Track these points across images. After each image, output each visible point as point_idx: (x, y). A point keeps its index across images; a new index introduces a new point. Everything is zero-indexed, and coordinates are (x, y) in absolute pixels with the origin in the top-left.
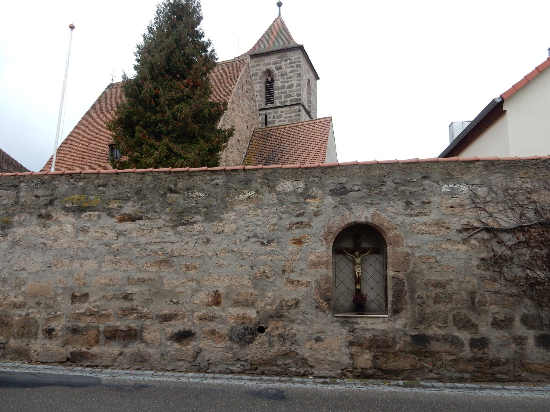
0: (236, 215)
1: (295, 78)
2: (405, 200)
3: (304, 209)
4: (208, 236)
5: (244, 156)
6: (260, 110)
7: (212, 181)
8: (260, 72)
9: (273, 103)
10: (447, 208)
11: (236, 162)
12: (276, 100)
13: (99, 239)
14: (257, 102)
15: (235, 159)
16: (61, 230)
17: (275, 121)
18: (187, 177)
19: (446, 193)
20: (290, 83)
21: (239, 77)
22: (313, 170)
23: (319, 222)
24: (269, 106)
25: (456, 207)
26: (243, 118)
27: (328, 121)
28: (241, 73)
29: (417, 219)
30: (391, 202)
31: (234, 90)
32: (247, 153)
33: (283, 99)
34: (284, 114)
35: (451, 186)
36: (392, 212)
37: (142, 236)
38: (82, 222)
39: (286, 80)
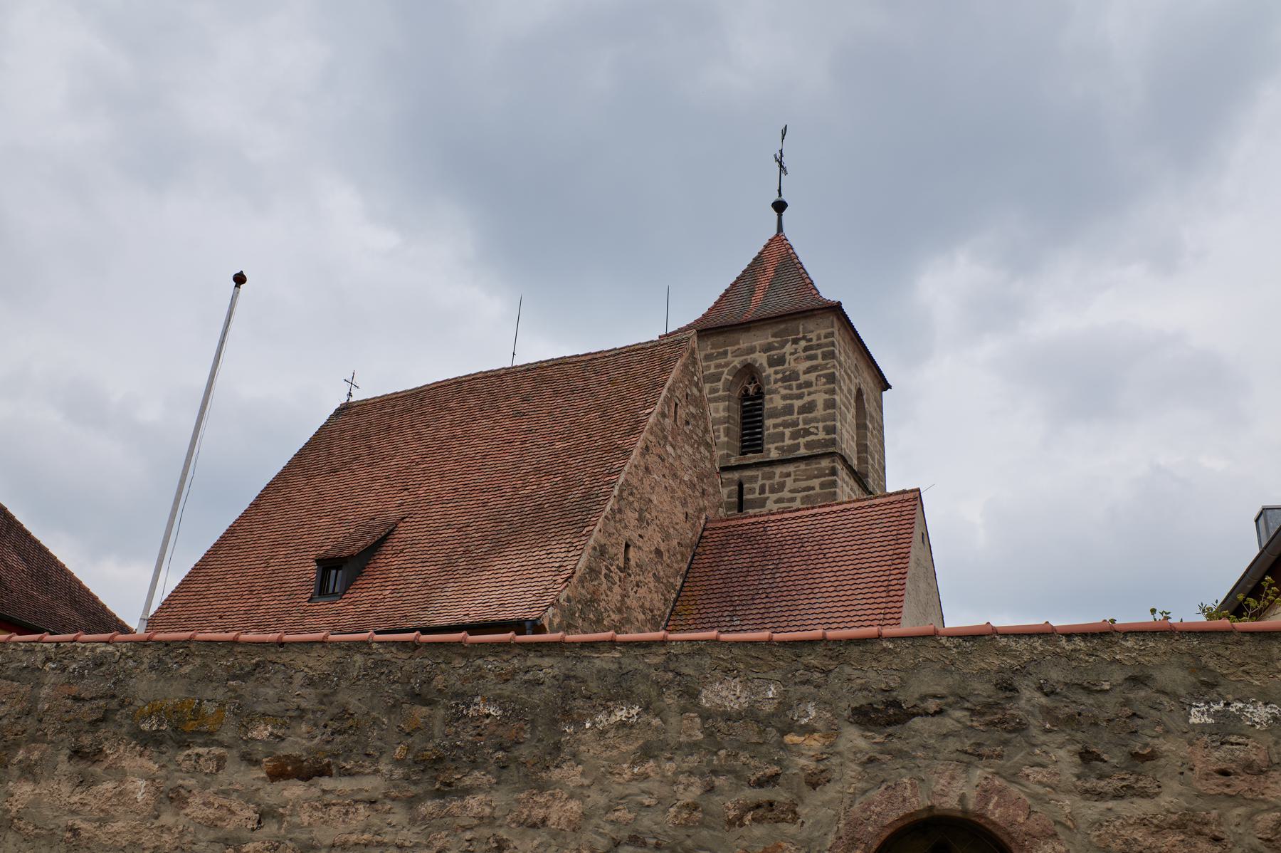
0: (583, 774)
1: (822, 385)
2: (1078, 747)
3: (779, 762)
4: (503, 833)
5: (674, 596)
6: (724, 469)
7: (527, 672)
8: (726, 370)
9: (761, 451)
10: (1208, 775)
11: (652, 611)
12: (768, 443)
13: (212, 825)
14: (714, 448)
15: (647, 604)
16: (121, 793)
17: (768, 498)
18: (460, 660)
19: (1203, 728)
20: (807, 399)
21: (667, 385)
22: (806, 651)
23: (824, 804)
24: (749, 459)
25: (1236, 773)
26: (673, 491)
27: (913, 498)
28: (672, 376)
29: (1121, 807)
30: (1037, 751)
31: (651, 419)
32: (682, 586)
33: (788, 442)
34: (789, 481)
35: (1216, 707)
36: (1040, 783)
37: (326, 822)
38: (177, 774)
39: (795, 391)
